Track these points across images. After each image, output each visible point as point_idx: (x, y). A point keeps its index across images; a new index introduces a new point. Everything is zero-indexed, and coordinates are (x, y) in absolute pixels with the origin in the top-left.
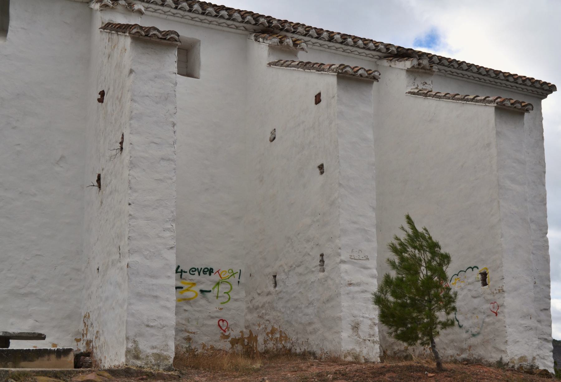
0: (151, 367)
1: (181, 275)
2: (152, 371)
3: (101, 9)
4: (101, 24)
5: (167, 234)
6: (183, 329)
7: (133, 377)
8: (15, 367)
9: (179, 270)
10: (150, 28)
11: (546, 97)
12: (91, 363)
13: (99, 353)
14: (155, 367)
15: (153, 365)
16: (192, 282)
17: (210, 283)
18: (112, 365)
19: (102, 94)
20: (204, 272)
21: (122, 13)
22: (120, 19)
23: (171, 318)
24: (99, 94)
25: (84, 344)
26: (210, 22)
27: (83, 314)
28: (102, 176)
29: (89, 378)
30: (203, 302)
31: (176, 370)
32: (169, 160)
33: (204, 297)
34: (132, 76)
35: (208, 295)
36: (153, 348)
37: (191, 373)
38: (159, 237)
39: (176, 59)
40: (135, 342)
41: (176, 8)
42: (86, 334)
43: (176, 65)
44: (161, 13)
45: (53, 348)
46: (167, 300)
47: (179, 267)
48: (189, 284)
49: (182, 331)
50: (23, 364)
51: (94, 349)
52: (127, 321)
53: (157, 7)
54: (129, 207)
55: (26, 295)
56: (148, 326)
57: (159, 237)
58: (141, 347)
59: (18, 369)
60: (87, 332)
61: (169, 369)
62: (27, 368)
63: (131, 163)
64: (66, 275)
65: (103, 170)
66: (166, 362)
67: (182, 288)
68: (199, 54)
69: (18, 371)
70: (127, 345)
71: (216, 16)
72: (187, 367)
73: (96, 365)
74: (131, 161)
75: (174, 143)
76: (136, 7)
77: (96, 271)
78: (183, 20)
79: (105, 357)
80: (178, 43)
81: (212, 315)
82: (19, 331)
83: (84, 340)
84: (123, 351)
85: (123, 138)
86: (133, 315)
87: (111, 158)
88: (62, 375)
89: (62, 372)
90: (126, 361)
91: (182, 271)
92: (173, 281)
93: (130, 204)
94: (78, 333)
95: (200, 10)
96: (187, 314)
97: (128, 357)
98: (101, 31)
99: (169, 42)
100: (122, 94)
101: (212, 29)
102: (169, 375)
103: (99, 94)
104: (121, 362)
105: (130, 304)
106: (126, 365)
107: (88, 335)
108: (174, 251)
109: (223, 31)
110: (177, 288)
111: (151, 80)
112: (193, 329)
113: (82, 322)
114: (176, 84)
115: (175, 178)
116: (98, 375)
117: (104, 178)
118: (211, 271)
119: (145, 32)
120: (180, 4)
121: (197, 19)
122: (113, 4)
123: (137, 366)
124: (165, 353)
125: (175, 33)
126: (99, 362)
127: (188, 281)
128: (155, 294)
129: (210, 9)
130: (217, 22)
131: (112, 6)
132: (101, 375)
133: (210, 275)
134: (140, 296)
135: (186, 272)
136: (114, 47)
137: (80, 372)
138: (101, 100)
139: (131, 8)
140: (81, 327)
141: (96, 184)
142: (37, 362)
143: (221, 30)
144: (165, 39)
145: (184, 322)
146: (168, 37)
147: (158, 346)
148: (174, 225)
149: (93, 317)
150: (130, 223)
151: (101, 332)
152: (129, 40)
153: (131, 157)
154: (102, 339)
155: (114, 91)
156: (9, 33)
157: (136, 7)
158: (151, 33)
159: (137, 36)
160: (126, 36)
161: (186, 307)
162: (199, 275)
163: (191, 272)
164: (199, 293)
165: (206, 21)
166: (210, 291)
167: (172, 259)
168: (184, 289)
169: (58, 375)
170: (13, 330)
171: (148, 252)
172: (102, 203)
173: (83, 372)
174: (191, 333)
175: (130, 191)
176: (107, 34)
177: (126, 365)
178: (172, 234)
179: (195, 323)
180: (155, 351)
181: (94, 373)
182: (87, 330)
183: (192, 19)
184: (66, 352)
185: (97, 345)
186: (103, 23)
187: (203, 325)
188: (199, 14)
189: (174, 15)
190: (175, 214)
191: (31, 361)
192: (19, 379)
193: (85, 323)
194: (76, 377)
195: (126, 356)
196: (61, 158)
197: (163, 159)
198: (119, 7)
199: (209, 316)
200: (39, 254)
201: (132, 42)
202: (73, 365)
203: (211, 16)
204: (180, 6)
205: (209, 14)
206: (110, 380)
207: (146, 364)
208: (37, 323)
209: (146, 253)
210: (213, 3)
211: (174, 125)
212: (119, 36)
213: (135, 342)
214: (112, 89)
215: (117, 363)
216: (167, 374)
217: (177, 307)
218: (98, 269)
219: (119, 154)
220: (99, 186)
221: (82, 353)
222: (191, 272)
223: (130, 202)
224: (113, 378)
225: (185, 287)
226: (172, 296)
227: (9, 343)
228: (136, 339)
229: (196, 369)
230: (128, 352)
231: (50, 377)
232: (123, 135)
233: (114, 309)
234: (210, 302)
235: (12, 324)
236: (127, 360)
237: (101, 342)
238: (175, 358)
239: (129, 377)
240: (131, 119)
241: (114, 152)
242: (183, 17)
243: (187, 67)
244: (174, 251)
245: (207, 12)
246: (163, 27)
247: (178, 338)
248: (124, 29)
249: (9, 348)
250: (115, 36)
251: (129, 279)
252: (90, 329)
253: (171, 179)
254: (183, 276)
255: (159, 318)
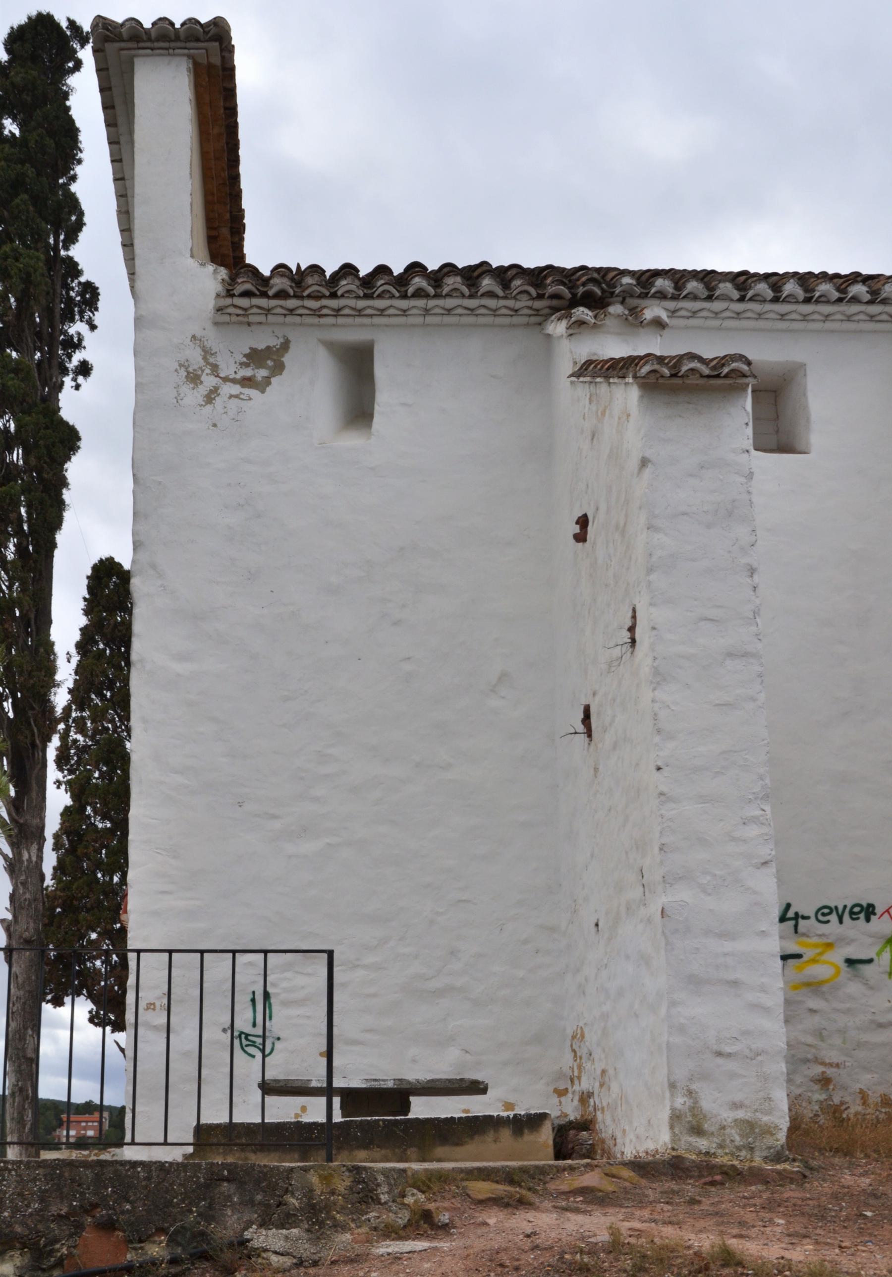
0: (732, 1154)
1: (796, 926)
2: (736, 1163)
3: (571, 331)
4: (571, 365)
5: (753, 831)
6: (809, 1056)
7: (691, 1177)
8: (424, 1160)
9: (791, 914)
10: (681, 358)
11: (63, 483)
12: (592, 1145)
13: (608, 1121)
14: (743, 1153)
15: (739, 1149)
16: (825, 940)
17: (870, 940)
18: (641, 1149)
19: (583, 522)
20: (853, 915)
21: (619, 334)
22: (615, 348)
23: (774, 1033)
24: (577, 523)
25: (576, 1102)
26: (827, 317)
27: (569, 1032)
28: (593, 710)
29: (585, 1184)
30: (854, 988)
31: (794, 1160)
32: (745, 655)
33: (858, 976)
34: (648, 471)
35: (866, 969)
36: (736, 1106)
37: (833, 1165)
38: (734, 839)
39: (69, 463)
40: (690, 1093)
41: (742, 299)
42: (579, 1078)
43: (749, 431)
44: (706, 318)
45: (504, 1114)
46: (763, 989)
47: (788, 906)
48: (816, 946)
49: (806, 1061)
50: (440, 1151)
51: (599, 1114)
52: (668, 1043)
53: (698, 305)
54: (657, 775)
55: (439, 993)
56: (719, 1054)
57: (734, 839)
58: (706, 1105)
59: (426, 1165)
60: (580, 1072)
61: (778, 1158)
62: (449, 1161)
63: (656, 672)
64: (525, 942)
65: (594, 694)
66: (769, 1141)
67: (798, 956)
68: (805, 395)
69: (426, 1170)
70: (672, 1101)
71: (840, 300)
72: (821, 1150)
73: (603, 1150)
74: (655, 668)
75: (756, 613)
76: (648, 314)
77: (593, 929)
78: (761, 324)
79: (624, 1131)
80: (751, 380)
81: (882, 1019)
82: (429, 1077)
83: (574, 1092)
84: (665, 1115)
85: (634, 617)
86: (682, 1029)
87: (610, 666)
88: (525, 1177)
89: (524, 1170)
90: (673, 1141)
91: (797, 916)
92: (772, 941)
93: (659, 769)
94: (561, 1075)
95: (800, 294)
96: (817, 1018)
97: (677, 1131)
98: (572, 383)
99: (728, 381)
100: (626, 516)
101: (832, 331)
102: (779, 1173)
103: (577, 523)
104: (661, 1143)
105: (673, 1004)
106: (673, 1149)
107: (584, 1079)
108: (772, 869)
109: (861, 331)
110: (784, 958)
111: (691, 475)
112: (833, 1056)
113: (568, 1049)
114: (750, 476)
115: (762, 697)
116: (606, 1174)
117: (599, 714)
118: (869, 911)
119: (670, 368)
120: (750, 288)
121: (391, 311)
122: (595, 317)
123: (700, 1153)
124: (765, 1119)
125: (692, 356)
126: (612, 1143)
127: (815, 940)
128: (732, 977)
129: (825, 287)
130: (842, 313)
131: (593, 321)
132: (613, 1176)
133: (868, 920)
134: (696, 983)
135: (808, 918)
136: (604, 413)
137: (564, 1170)
138: (581, 537)
139: (636, 318)
140: (567, 1060)
141: (581, 728)
142: (470, 1147)
143: (855, 332)
144: (718, 376)
145: (810, 1040)
146: (726, 370)
147: (747, 1102)
148: (767, 808)
149: (592, 1037)
150: (663, 812)
151: (611, 1072)
152: (634, 393)
153: (655, 659)
154: (615, 1087)
155: (608, 511)
156: (377, 419)
157: (648, 314)
158: (684, 368)
159: (652, 379)
160: (626, 384)
161: (813, 1003)
162: (841, 922)
163: (821, 918)
164: (843, 966)
165: (816, 316)
166: (870, 961)
167: (768, 892)
168: (805, 958)
169: (516, 1178)
170: (415, 1074)
171: (708, 878)
172: (596, 770)
173: (572, 1169)
174: (831, 1065)
175: (657, 739)
176: (587, 385)
177: (673, 1149)
178: (765, 830)
179: (837, 1041)
180: (740, 1114)
181: (597, 1170)
182: (580, 1067)
183: (783, 317)
184: (535, 1121)
185: (605, 1104)
186: (575, 363)
187: (859, 1045)
188: (797, 302)
189: (738, 315)
190: (768, 781)
191: (457, 1144)
192: (429, 1187)
193: (574, 1051)
194: (558, 1182)
195: (672, 1127)
196: (500, 679)
197: (730, 655)
198: (608, 322)
199: (872, 1022)
200: (464, 898)
201: (641, 397)
202: (551, 1150)
203: (828, 302)
204: (750, 294)
205: (823, 300)
206: (635, 1186)
207: (721, 1146)
208: (468, 1057)
209: (705, 880)
210: (831, 272)
211: (752, 571)
212: (613, 387)
213: (690, 1093)
214: (603, 507)
215: (651, 1146)
216: (772, 1171)
217: (788, 1002)
218: (597, 925)
219: (629, 653)
220: (589, 733)
221: (571, 1122)
222: (821, 918)
223: (660, 764)
224: (644, 1182)
225: (808, 954)
226: (773, 981)
227: (408, 1104)
228: (694, 1087)
229: (846, 1155)
230: (676, 1117)
231: (497, 1182)
232: (634, 611)
233: (637, 1016)
234: (871, 988)
235: (414, 1061)
236: (675, 1138)
237: (614, 1096)
238: (794, 1128)
239: (680, 1178)
240: (650, 570)
241: (617, 652)
242: (760, 316)
243: (777, 432)
244: (772, 869)
245: (817, 294)
246: (711, 349)
247: (799, 1079)
248: (621, 368)
249: (411, 1116)
250: (603, 388)
251: (667, 943)
252: (588, 1065)
253: (753, 699)
254: (801, 929)
255: (746, 1033)
